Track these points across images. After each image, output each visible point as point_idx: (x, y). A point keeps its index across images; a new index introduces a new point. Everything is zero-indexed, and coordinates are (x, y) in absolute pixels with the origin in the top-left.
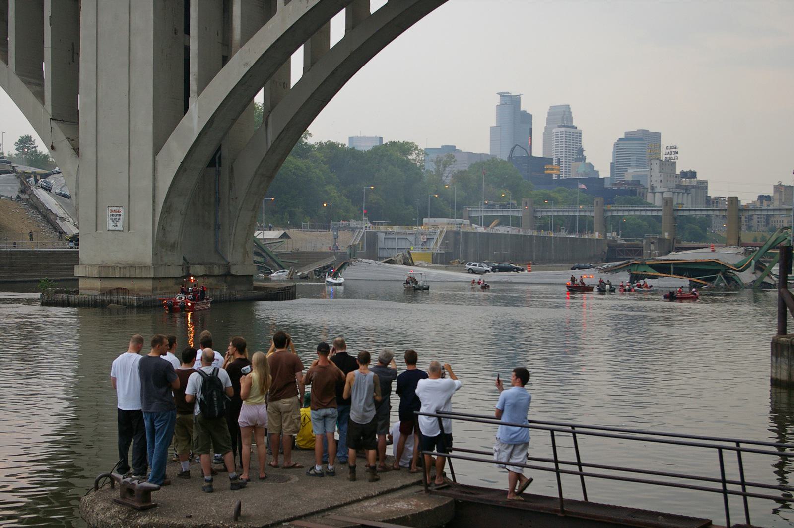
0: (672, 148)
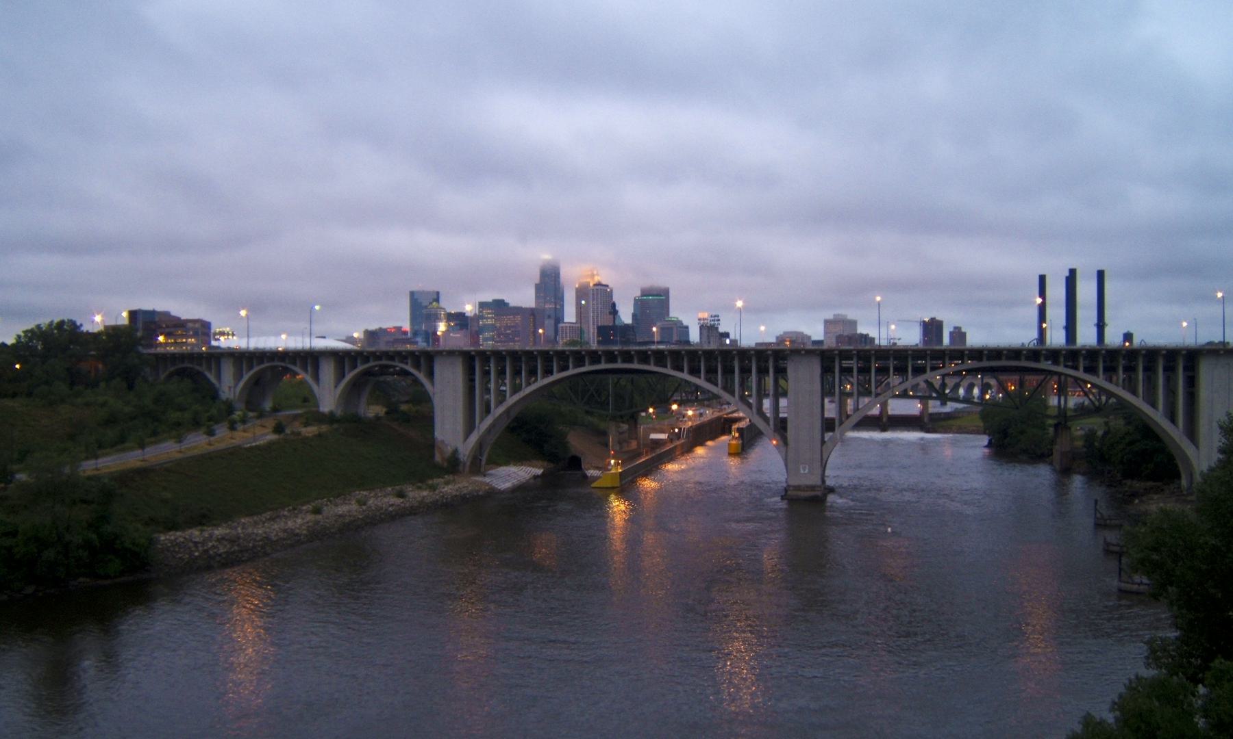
0: (715, 316)
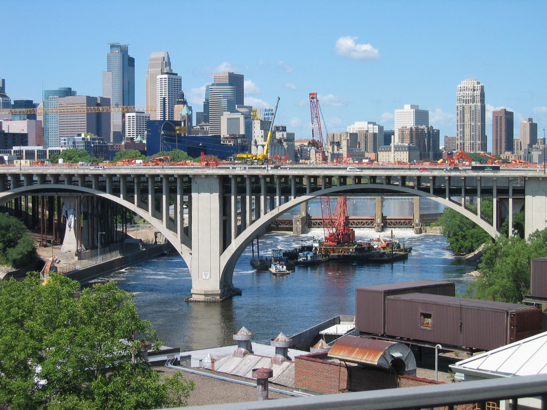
0: (269, 110)
